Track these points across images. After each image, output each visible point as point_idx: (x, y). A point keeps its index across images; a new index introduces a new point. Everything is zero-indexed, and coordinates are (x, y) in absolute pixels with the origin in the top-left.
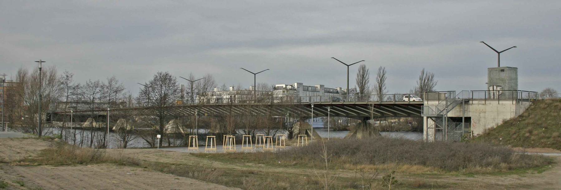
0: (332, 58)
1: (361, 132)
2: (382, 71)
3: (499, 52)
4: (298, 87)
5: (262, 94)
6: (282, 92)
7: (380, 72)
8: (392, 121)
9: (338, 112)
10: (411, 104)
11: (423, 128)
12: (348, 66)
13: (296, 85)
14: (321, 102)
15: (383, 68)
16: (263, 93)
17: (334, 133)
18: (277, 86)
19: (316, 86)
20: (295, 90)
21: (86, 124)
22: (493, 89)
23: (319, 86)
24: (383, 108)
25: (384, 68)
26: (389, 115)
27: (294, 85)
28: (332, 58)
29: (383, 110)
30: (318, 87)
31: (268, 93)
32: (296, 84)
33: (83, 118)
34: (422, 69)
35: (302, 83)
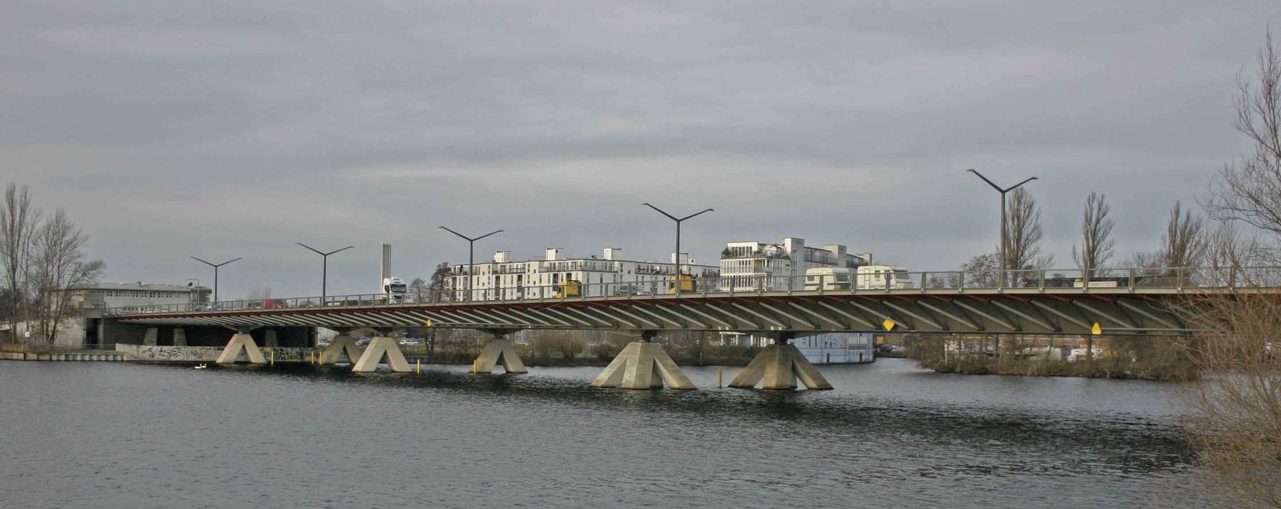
0: (970, 171)
1: (776, 365)
2: (1096, 206)
3: (679, 219)
4: (794, 251)
5: (639, 269)
6: (752, 265)
7: (1092, 209)
8: (970, 338)
9: (618, 319)
10: (1047, 294)
11: (253, 338)
12: (679, 221)
13: (788, 246)
14: (608, 297)
15: (1098, 196)
16: (642, 268)
17: (934, 381)
18: (731, 245)
19: (826, 248)
20: (787, 258)
21: (228, 354)
22: (615, 280)
23: (834, 250)
24: (637, 310)
25: (1103, 197)
26: (1003, 326)
27: (784, 245)
28: (970, 171)
29: (637, 315)
30: (833, 251)
31: (653, 267)
32: (788, 243)
33: (218, 336)
34: (1176, 203)
35: (803, 240)
